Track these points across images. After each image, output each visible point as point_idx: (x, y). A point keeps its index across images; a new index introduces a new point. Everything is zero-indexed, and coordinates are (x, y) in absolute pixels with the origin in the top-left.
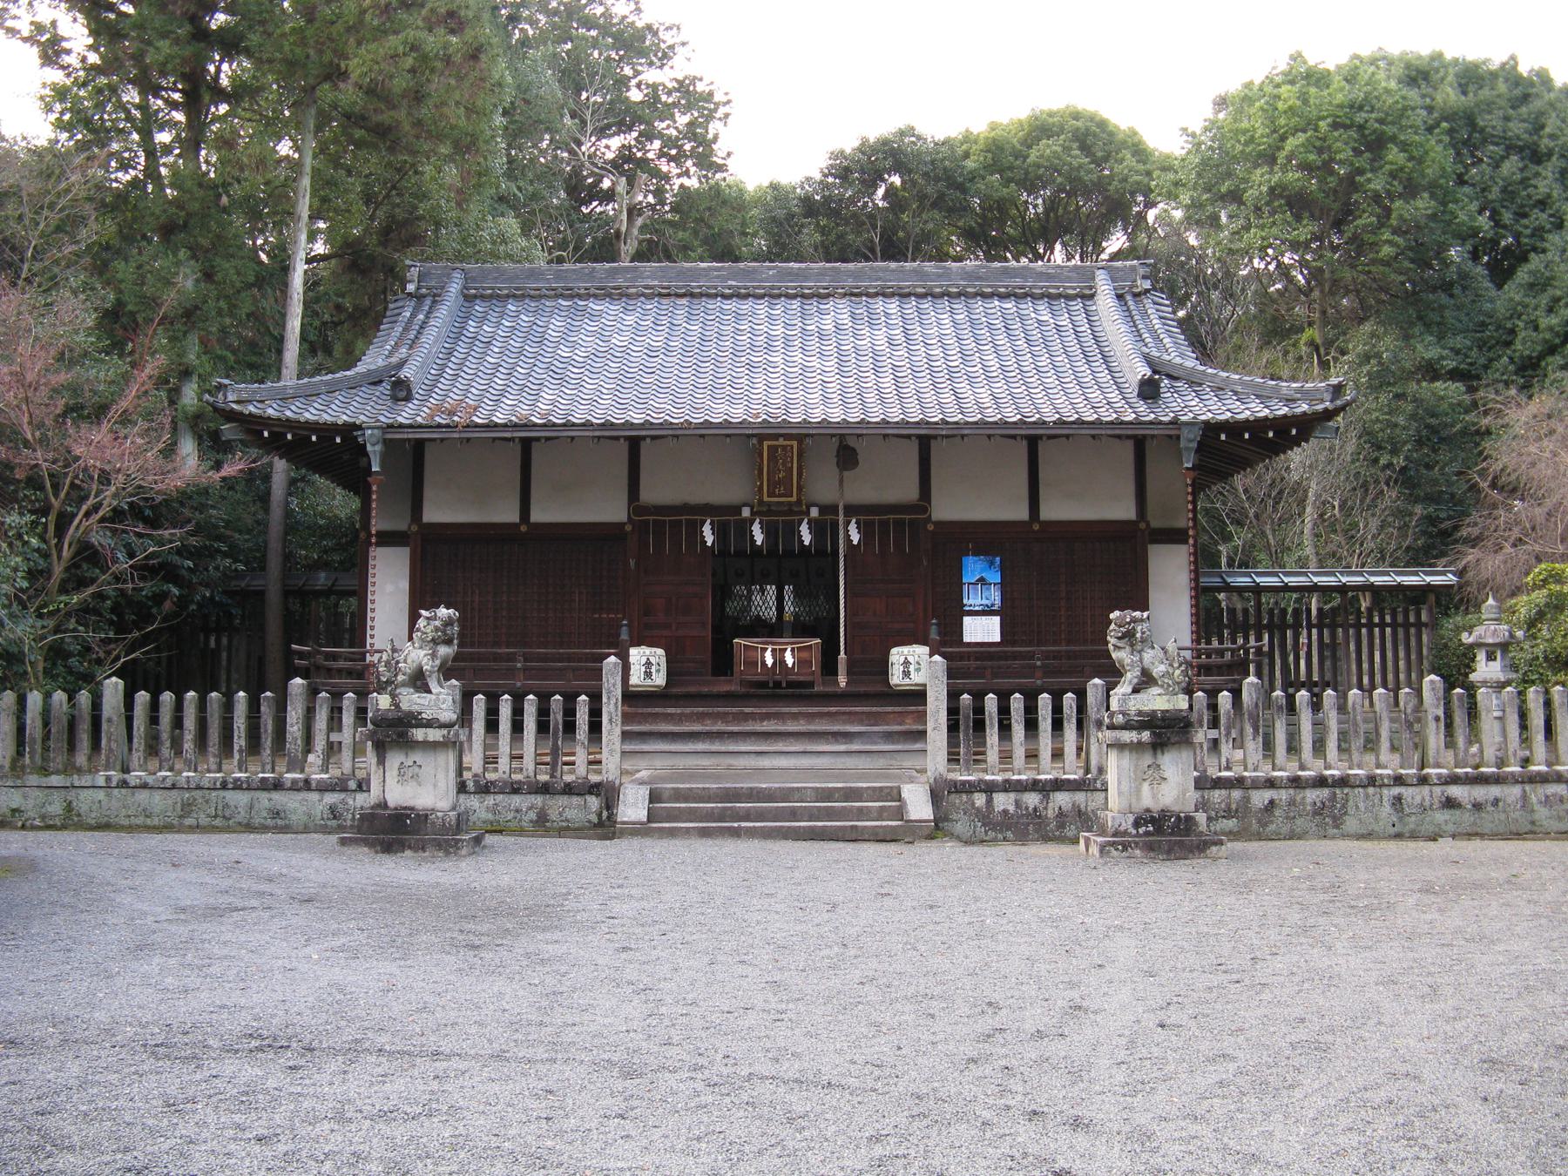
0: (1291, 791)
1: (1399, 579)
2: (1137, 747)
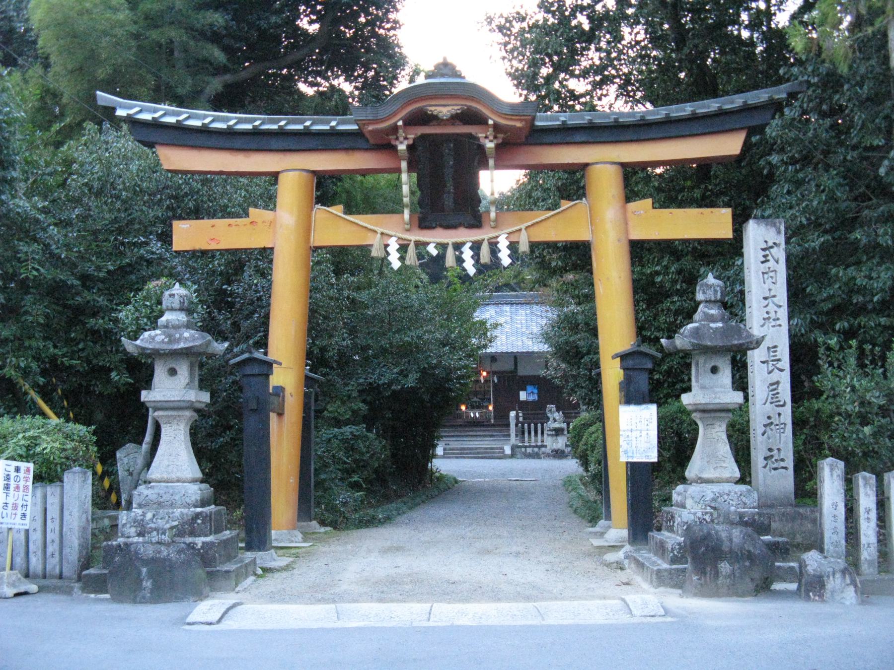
2: (552, 435)
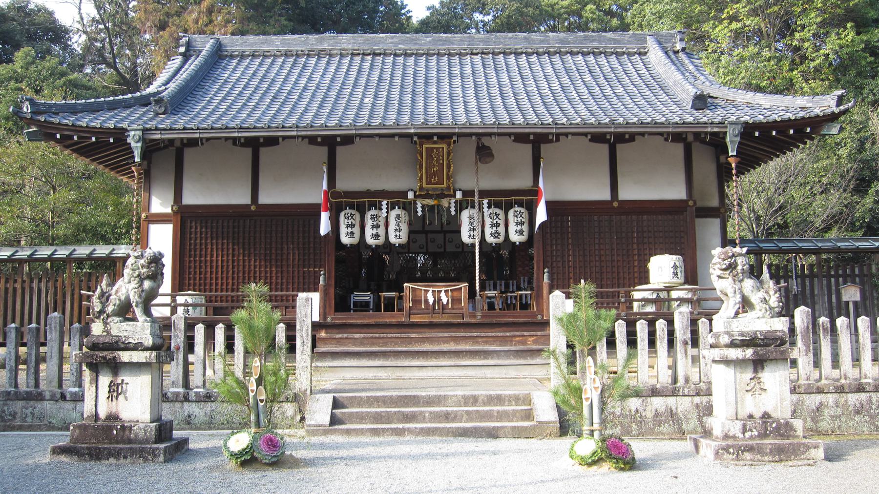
0: (835, 395)
1: (857, 244)
